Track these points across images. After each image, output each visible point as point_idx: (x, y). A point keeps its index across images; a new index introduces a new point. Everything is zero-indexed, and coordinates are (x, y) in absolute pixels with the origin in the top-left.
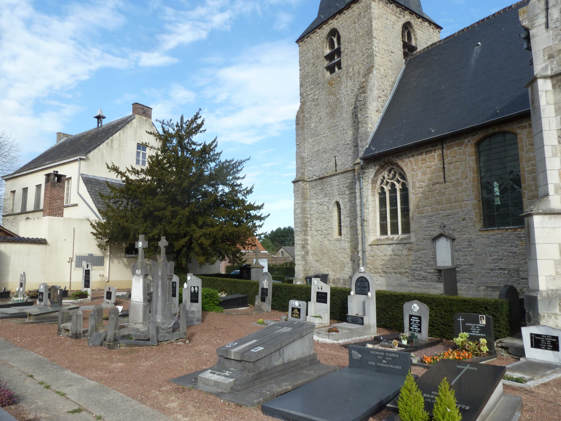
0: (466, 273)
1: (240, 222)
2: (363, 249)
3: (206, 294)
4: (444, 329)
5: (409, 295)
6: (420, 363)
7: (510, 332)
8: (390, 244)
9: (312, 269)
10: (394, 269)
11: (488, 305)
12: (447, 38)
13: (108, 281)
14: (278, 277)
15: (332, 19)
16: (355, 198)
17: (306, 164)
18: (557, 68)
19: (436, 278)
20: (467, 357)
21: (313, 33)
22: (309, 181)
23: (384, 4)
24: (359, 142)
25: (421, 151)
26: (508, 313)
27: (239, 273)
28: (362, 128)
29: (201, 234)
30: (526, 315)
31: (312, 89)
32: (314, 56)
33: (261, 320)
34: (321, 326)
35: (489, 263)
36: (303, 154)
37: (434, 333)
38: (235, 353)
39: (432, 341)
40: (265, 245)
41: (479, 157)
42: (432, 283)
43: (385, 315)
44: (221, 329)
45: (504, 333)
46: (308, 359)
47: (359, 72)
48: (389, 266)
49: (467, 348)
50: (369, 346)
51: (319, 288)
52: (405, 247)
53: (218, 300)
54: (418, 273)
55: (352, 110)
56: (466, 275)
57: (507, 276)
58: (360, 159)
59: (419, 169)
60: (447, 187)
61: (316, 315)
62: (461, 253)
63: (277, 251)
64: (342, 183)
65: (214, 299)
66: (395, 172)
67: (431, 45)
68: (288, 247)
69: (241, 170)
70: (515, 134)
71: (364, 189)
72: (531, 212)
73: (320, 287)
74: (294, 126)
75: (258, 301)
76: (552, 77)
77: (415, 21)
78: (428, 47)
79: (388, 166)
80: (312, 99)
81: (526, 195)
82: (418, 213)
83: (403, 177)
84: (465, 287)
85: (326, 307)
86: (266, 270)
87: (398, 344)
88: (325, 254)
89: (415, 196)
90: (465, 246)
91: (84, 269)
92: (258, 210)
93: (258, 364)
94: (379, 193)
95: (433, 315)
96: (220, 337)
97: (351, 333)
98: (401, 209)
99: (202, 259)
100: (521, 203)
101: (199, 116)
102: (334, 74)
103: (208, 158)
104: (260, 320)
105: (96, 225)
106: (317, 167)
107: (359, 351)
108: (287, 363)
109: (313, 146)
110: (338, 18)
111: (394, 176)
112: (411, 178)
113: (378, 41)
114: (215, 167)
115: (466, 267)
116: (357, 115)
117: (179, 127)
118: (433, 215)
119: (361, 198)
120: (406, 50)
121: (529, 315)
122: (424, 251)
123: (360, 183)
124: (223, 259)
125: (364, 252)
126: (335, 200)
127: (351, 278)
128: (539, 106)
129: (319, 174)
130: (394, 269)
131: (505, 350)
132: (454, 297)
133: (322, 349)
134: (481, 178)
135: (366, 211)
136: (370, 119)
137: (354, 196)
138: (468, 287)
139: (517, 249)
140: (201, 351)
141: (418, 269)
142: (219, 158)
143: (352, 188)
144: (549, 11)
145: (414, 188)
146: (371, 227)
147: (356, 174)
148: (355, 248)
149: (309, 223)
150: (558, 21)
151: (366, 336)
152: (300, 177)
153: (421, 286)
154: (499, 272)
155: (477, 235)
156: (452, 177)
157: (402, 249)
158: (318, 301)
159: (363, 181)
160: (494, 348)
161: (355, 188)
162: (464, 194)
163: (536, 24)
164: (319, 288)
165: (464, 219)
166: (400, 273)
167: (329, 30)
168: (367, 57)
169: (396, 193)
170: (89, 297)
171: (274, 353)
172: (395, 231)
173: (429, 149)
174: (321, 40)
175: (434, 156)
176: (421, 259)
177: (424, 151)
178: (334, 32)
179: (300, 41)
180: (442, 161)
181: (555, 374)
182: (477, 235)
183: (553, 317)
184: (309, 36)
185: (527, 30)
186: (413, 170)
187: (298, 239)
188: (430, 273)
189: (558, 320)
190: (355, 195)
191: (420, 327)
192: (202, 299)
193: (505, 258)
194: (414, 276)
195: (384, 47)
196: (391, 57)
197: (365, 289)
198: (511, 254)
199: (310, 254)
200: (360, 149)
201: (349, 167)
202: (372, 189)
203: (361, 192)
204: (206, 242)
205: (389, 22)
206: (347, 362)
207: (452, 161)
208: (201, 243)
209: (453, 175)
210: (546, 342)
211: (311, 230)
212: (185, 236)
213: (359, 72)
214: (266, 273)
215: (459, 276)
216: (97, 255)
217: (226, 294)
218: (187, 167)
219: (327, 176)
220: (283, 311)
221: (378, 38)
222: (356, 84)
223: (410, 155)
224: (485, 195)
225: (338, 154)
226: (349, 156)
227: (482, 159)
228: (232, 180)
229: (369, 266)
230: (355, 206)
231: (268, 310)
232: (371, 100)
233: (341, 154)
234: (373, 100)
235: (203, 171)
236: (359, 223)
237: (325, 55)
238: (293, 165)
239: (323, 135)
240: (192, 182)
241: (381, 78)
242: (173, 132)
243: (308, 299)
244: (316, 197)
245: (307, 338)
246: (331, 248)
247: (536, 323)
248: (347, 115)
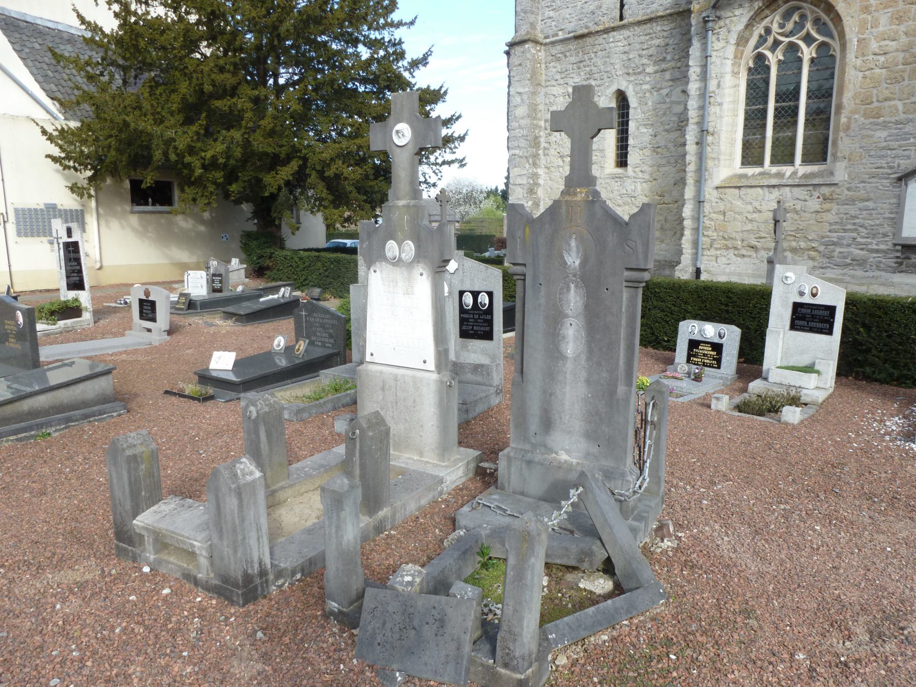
8: (774, 186)
13: (100, 268)
19: (891, 262)
22: (546, 44)
42: (879, 273)
48: (763, 235)
52: (816, 194)
54: (842, 250)
59: (885, 8)
64: (638, 46)
66: (803, 17)
71: (714, 59)
89: (861, 74)
91: (61, 241)
94: (750, 69)
105: (55, 133)
106: (569, 11)
111: (800, 26)
119: (704, 76)
122: (866, 203)
126: (614, 88)
129: (574, 26)
135: (713, 110)
141: (845, 242)
146: (723, 147)
149: (542, 140)
152: (528, 33)
153: (848, 279)
157: (807, 198)
159: (714, 38)
170: (87, 316)
172: (784, 155)
176: (857, 221)
188: (877, 251)
201: (661, 8)
202: (735, 57)
208: (337, 176)
216: (67, 208)
219: (597, 32)
229: (710, 233)
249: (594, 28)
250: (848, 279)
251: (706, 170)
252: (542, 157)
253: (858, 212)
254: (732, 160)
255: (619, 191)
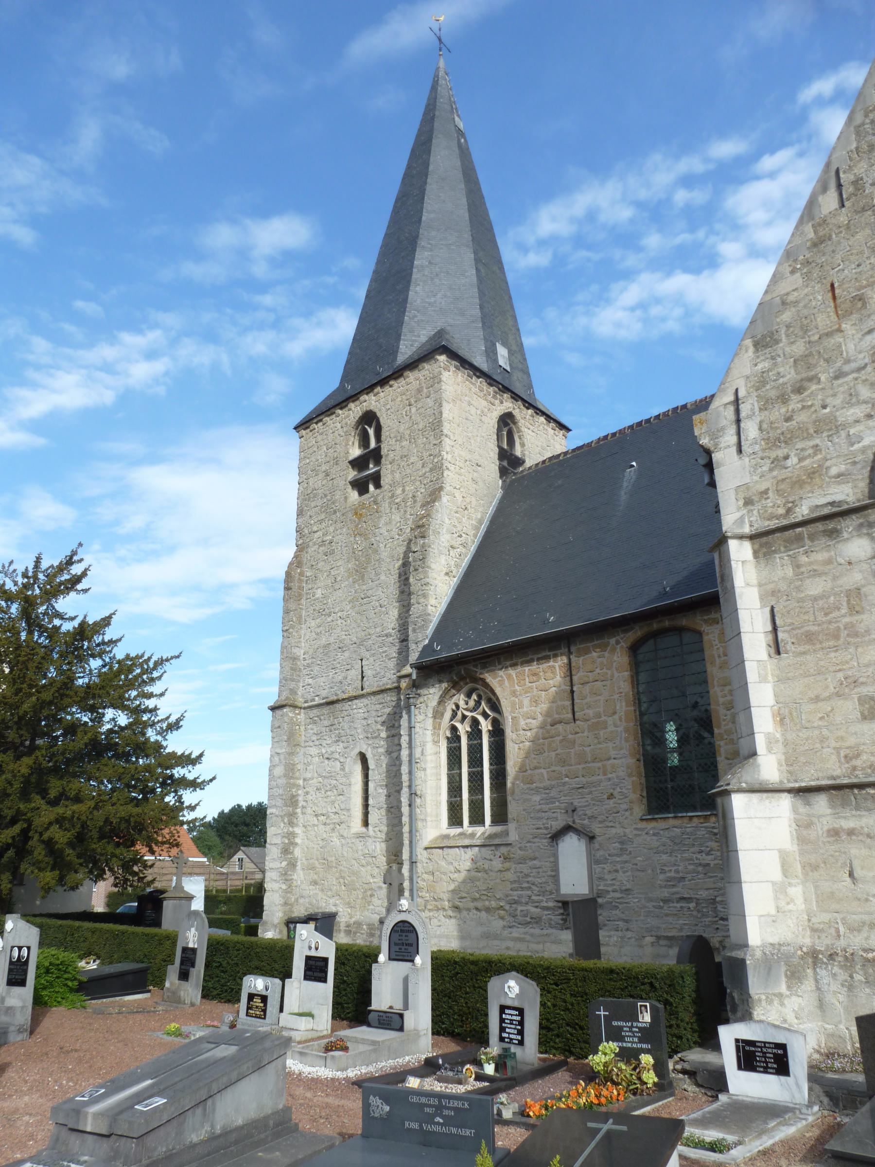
0: (616, 907)
1: (147, 792)
2: (411, 857)
3: (47, 964)
4: (571, 1035)
5: (500, 961)
6: (519, 1119)
7: (699, 1037)
8: (467, 847)
9: (301, 901)
10: (474, 900)
11: (656, 978)
12: (578, 448)
14: (225, 920)
15: (367, 394)
16: (398, 748)
17: (300, 670)
18: (759, 522)
20: (614, 1098)
21: (329, 416)
22: (305, 708)
23: (466, 376)
24: (410, 632)
25: (530, 657)
26: (694, 995)
27: (134, 911)
28: (416, 606)
29: (52, 817)
30: (728, 999)
31: (321, 521)
32: (328, 459)
33: (173, 1026)
34: (310, 1035)
35: (661, 887)
36: (295, 650)
37: (552, 1044)
38: (97, 1115)
39: (548, 1063)
40: (203, 845)
41: (637, 673)
42: (550, 931)
43: (450, 1008)
44: (76, 1051)
45: (688, 1040)
46: (271, 1123)
47: (414, 496)
48: (464, 895)
49: (614, 1077)
50: (413, 1082)
51: (310, 948)
52: (498, 854)
53: (75, 979)
55: (399, 569)
56: (617, 912)
57: (695, 913)
58: (412, 666)
59: (526, 693)
60: (577, 730)
61: (301, 1011)
62: (608, 867)
63: (230, 857)
64: (374, 714)
65: (66, 976)
66: (480, 697)
67: (550, 459)
68: (253, 850)
69: (159, 678)
70: (700, 634)
71: (417, 729)
72: (728, 788)
73: (313, 946)
74: (281, 593)
75: (172, 979)
76: (752, 538)
77: (521, 412)
78: (544, 462)
79: (467, 684)
80: (320, 540)
81: (722, 750)
82: (523, 781)
83: (495, 706)
84: (615, 939)
85: (325, 991)
86: (198, 905)
87: (476, 1073)
88: (331, 867)
89: (516, 746)
90: (615, 852)
92: (190, 767)
93: (150, 1141)
94: (448, 738)
95: (549, 1004)
96: (72, 1070)
97: (375, 1050)
98: (491, 772)
99: (49, 876)
100: (715, 765)
101: (75, 558)
102: (366, 496)
103: (88, 648)
104: (173, 1025)
106: (323, 679)
107: (386, 1098)
108: (220, 1136)
109: (317, 634)
110: (378, 393)
112: (509, 709)
113: (453, 443)
114: (100, 670)
115: (618, 895)
116: (407, 579)
117: (28, 577)
118: (553, 787)
120: (505, 463)
121: (733, 998)
122: (535, 862)
123: (410, 717)
124: (100, 877)
125: (413, 863)
126: (357, 751)
127: (382, 922)
128: (733, 587)
129: (327, 693)
130: (474, 900)
131: (689, 1078)
132: (590, 964)
133: (309, 1095)
134: (642, 714)
136: (432, 588)
137: (396, 742)
138: (622, 938)
139: (710, 857)
140: (16, 1111)
141: (523, 900)
142: (111, 651)
143: (393, 726)
144: (742, 425)
145: (515, 729)
146: (429, 810)
147: (402, 697)
148: (394, 856)
149: (300, 798)
150: (756, 443)
151: (407, 1058)
152: (287, 698)
153: (528, 937)
154: (678, 905)
155: (636, 829)
156: (587, 711)
157: (492, 857)
158: (307, 978)
159: (417, 712)
160: (668, 1073)
161: (400, 726)
162: (610, 745)
163: (722, 445)
164: (310, 948)
165: (611, 796)
166: (488, 910)
167: (360, 414)
168: (431, 470)
169: (481, 739)
171: (190, 1112)
172: (477, 818)
173: (544, 654)
174: (345, 429)
175: (554, 667)
176: (530, 879)
177: (536, 657)
178: (369, 418)
179: (304, 427)
180: (568, 679)
181: (784, 1128)
182: (636, 829)
183: (776, 1002)
184: (321, 420)
185: (708, 453)
186: (514, 693)
187: (274, 832)
188: (547, 908)
189: (785, 1007)
190: (399, 739)
191: (521, 1032)
192: (38, 977)
193: (689, 876)
194: (514, 916)
195: (463, 454)
196: (475, 474)
197: (410, 949)
198: (700, 869)
199: (299, 867)
200: (412, 646)
202: (434, 728)
203: (410, 735)
204: (61, 837)
205: (473, 411)
206: (355, 1125)
207: (586, 679)
208: (50, 840)
209: (589, 707)
210: (765, 1057)
211: (303, 813)
212: (13, 822)
213: (414, 496)
214: (196, 913)
215: (604, 914)
217: (98, 962)
218: (37, 667)
219: (343, 699)
220: (229, 1001)
221: (452, 437)
222: (409, 519)
223: (508, 663)
224: (649, 748)
225: (367, 654)
226: (390, 659)
227: (643, 677)
228: (135, 698)
229: (423, 894)
230: (397, 763)
231: (193, 1000)
232: (436, 551)
233: (373, 655)
234: (441, 553)
235: (72, 680)
236: (404, 799)
237: (351, 458)
238: (273, 671)
239: (339, 614)
240: (44, 702)
241: (456, 512)
242: (14, 589)
243: (285, 974)
244: (317, 743)
245: (271, 1069)
246: (345, 854)
247: (746, 1016)
248: (389, 579)
249: (342, 696)
250: (528, 937)
251: (417, 831)
252: (300, 815)
253: (530, 871)
254: (438, 821)
255: (362, 850)
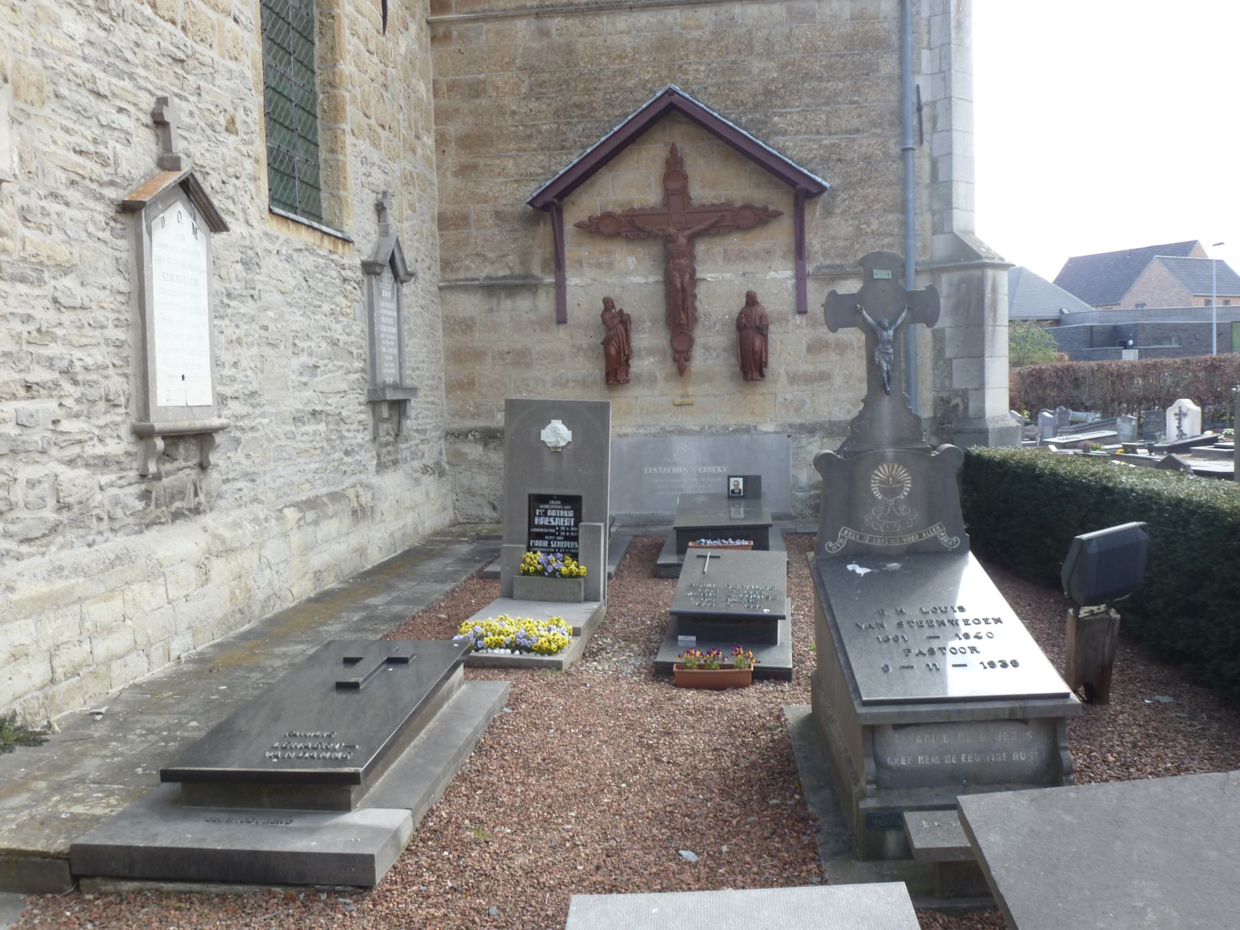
176: (53, 350)
188: (104, 463)
